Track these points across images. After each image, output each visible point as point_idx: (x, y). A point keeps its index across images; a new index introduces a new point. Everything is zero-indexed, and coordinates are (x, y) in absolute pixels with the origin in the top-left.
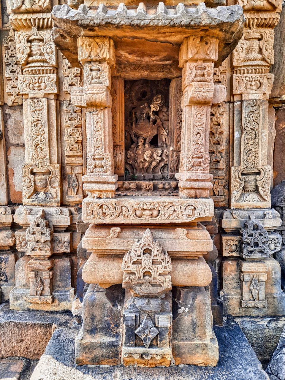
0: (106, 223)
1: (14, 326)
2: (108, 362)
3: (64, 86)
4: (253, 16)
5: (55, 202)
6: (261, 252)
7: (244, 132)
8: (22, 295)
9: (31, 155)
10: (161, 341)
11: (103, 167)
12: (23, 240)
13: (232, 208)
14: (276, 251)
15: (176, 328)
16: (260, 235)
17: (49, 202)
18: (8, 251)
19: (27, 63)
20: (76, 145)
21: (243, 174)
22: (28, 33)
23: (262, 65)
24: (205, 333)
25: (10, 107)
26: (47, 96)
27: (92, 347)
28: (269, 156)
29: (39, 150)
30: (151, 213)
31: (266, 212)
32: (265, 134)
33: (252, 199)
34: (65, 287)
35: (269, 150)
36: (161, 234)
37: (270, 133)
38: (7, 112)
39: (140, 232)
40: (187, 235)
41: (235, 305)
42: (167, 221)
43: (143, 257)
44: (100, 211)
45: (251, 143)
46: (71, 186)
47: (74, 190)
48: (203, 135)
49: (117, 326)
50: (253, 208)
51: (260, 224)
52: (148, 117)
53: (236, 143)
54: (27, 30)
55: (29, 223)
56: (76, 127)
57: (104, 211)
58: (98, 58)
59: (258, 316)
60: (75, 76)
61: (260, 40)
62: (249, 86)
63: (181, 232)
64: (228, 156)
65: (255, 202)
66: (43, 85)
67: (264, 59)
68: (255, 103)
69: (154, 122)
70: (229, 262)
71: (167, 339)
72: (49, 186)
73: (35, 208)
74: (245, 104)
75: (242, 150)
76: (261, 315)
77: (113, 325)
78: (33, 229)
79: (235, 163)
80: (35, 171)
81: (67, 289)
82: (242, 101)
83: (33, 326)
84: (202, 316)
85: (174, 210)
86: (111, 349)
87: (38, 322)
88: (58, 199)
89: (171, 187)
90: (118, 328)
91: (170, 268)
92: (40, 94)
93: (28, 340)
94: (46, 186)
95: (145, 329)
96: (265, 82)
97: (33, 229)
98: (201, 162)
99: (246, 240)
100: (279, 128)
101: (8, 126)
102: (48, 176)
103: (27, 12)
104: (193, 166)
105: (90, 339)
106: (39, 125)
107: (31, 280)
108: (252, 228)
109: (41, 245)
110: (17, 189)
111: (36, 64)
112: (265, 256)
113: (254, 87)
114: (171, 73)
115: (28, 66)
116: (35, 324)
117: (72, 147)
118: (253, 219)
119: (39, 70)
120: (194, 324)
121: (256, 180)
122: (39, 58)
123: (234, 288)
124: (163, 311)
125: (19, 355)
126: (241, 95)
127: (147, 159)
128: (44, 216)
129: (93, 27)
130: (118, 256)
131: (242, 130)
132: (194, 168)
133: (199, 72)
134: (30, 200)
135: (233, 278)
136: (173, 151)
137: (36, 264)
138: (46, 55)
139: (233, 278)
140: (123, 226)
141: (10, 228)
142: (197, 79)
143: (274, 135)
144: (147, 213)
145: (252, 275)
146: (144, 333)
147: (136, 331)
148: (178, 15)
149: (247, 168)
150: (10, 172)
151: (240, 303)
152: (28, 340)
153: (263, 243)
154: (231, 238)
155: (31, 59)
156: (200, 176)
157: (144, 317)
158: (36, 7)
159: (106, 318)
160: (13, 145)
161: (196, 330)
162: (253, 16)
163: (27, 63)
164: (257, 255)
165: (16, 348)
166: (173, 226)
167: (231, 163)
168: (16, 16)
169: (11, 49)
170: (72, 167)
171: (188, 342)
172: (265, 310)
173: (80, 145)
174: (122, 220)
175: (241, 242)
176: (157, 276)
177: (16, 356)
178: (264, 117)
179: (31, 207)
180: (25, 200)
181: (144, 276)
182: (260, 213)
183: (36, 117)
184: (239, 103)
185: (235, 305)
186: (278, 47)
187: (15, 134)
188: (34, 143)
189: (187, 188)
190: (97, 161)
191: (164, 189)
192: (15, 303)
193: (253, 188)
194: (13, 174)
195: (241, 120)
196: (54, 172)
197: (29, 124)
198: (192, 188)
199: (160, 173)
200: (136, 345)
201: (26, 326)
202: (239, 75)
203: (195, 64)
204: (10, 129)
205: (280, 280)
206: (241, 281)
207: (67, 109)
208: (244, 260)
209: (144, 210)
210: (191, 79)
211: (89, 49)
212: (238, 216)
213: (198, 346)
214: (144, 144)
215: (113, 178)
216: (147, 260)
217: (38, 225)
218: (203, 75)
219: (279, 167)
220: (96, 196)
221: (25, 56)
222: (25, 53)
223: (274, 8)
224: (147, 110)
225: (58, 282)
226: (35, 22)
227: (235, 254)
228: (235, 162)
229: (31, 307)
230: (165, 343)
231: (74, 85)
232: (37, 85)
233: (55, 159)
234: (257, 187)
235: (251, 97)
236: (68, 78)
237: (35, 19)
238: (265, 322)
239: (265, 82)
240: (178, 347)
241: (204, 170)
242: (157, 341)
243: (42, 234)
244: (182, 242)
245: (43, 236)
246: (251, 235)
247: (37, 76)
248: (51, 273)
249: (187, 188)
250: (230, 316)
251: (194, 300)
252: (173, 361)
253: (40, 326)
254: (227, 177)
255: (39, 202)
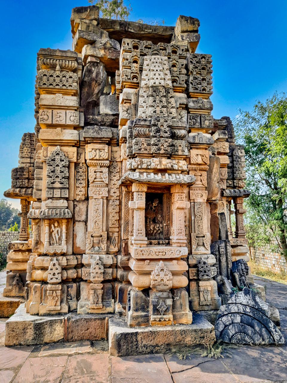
0: (144, 258)
1: (84, 320)
2: (144, 325)
3: (111, 193)
4: (197, 167)
5: (104, 252)
6: (207, 275)
7: (196, 217)
8: (85, 305)
9: (92, 227)
10: (168, 312)
11: (141, 233)
12: (87, 273)
13: (193, 254)
14: (214, 275)
15: (174, 306)
16: (207, 267)
17: (100, 252)
18: (71, 281)
19: (93, 182)
20: (116, 222)
21: (197, 237)
22: (95, 168)
23: (202, 187)
24: (186, 309)
25: (77, 201)
26: (102, 198)
27: (137, 317)
28: (208, 228)
29: (96, 224)
30: (162, 253)
31: (209, 256)
32: (205, 218)
33: (202, 250)
34: (108, 299)
35: (208, 225)
36: (167, 263)
37: (208, 216)
38: (75, 204)
39: (158, 262)
40: (177, 263)
41: (197, 305)
42: (169, 257)
43: (160, 273)
44: (141, 253)
45: (199, 222)
46: (112, 243)
47: (113, 245)
48: (182, 221)
49: (148, 307)
50: (202, 254)
51: (206, 261)
52: (151, 208)
53: (193, 222)
54: (94, 167)
55: (90, 263)
56: (116, 213)
57: (143, 253)
58: (142, 191)
59: (208, 310)
60: (117, 189)
61: (201, 176)
62: (197, 196)
63: (175, 262)
64: (189, 228)
65: (203, 251)
66: (101, 193)
67: (203, 184)
68: (200, 204)
69: (154, 211)
70: (193, 282)
71: (170, 311)
72: (101, 243)
73: (94, 255)
74: (196, 204)
75: (196, 225)
76: (209, 309)
77: (146, 307)
78: (95, 266)
79: (193, 232)
80: (93, 235)
81: (110, 300)
82: (194, 202)
83: (95, 319)
84: (184, 301)
85: (172, 253)
86: (145, 318)
87: (97, 317)
88: (106, 250)
89: (166, 243)
90: (148, 308)
91: (172, 277)
92: (100, 197)
93: (92, 328)
94: (99, 243)
95: (161, 306)
96: (204, 194)
97: (95, 266)
98: (181, 232)
99: (200, 270)
100: (212, 213)
101: (75, 211)
102: (101, 238)
103: (97, 160)
104: (179, 233)
105: (136, 314)
106: (97, 212)
107: (91, 295)
108: (203, 263)
109: (98, 275)
110: (78, 245)
111: (98, 183)
112: (209, 278)
113: (199, 197)
114: (164, 191)
115: (94, 183)
116: (96, 319)
117: (113, 223)
118: (203, 259)
119: (99, 185)
120: (181, 305)
121: (203, 240)
122: (100, 180)
123: (196, 295)
124: (168, 298)
125: (85, 338)
126: (194, 200)
127: (152, 229)
128: (100, 259)
129: (229, 269)
130: (148, 273)
131: (195, 216)
132: (179, 234)
133: (180, 197)
134: (90, 251)
135: (195, 290)
136: (166, 226)
137: (95, 286)
138: (103, 179)
139: (195, 290)
140: (151, 260)
141: (185, 245)
142: (179, 199)
143: (210, 217)
144: (161, 253)
145: (204, 287)
146: (161, 308)
147: (157, 308)
148: (174, 180)
149: (199, 234)
150: (74, 236)
151: (199, 303)
152: (92, 328)
153: (208, 271)
154: (193, 269)
155: (96, 180)
156: (182, 238)
157: (161, 301)
158: (101, 158)
159: (143, 304)
160: (77, 221)
161: (182, 307)
162: (197, 167)
163: (93, 182)
164: (206, 277)
165: (84, 334)
166: (171, 259)
167: (191, 232)
168: (90, 161)
169: (80, 172)
170: (113, 233)
171: (179, 313)
172: (211, 306)
173: (118, 222)
174: (150, 257)
175: (198, 271)
176: (166, 281)
177: (83, 339)
178: (205, 210)
179: (92, 255)
180: (87, 251)
181: (161, 281)
182: (206, 256)
183: (96, 207)
184: (193, 203)
185: (197, 305)
186: (209, 175)
187: (78, 215)
188: (94, 221)
189: (177, 243)
190: (139, 231)
191: (163, 244)
192: (81, 310)
193: (202, 244)
194: (76, 237)
195: (194, 211)
196: (104, 236)
197: (92, 211)
198: (179, 243)
199: (158, 236)
200: (157, 315)
201: (91, 320)
202: (192, 191)
203: (178, 194)
204: (76, 212)
205: (217, 291)
206: (199, 291)
207: (112, 204)
208: (200, 280)
209: (159, 252)
210: (177, 199)
211: (139, 187)
212: (196, 258)
213: (183, 314)
214: (150, 222)
215: (146, 239)
216: (162, 274)
217: (97, 264)
218: (181, 198)
219: (214, 233)
220: (139, 246)
221: (93, 178)
222: (93, 178)
223: (206, 164)
224: (151, 205)
225: (105, 297)
226: (99, 165)
227: (195, 278)
228: (193, 231)
229: (90, 311)
230: (170, 313)
231: (116, 193)
232: (98, 192)
233: (105, 229)
234: (203, 243)
235: (198, 201)
236: (113, 189)
237: (99, 163)
238: (211, 312)
239: (204, 194)
240: (175, 315)
241: (183, 235)
242: (166, 312)
243: (100, 269)
244: (175, 266)
245: (100, 270)
246: (202, 267)
247: (98, 189)
248: (103, 290)
249: (177, 243)
250: (195, 311)
251: (181, 293)
252: (173, 322)
253: (99, 320)
254: (189, 238)
255: (95, 252)
